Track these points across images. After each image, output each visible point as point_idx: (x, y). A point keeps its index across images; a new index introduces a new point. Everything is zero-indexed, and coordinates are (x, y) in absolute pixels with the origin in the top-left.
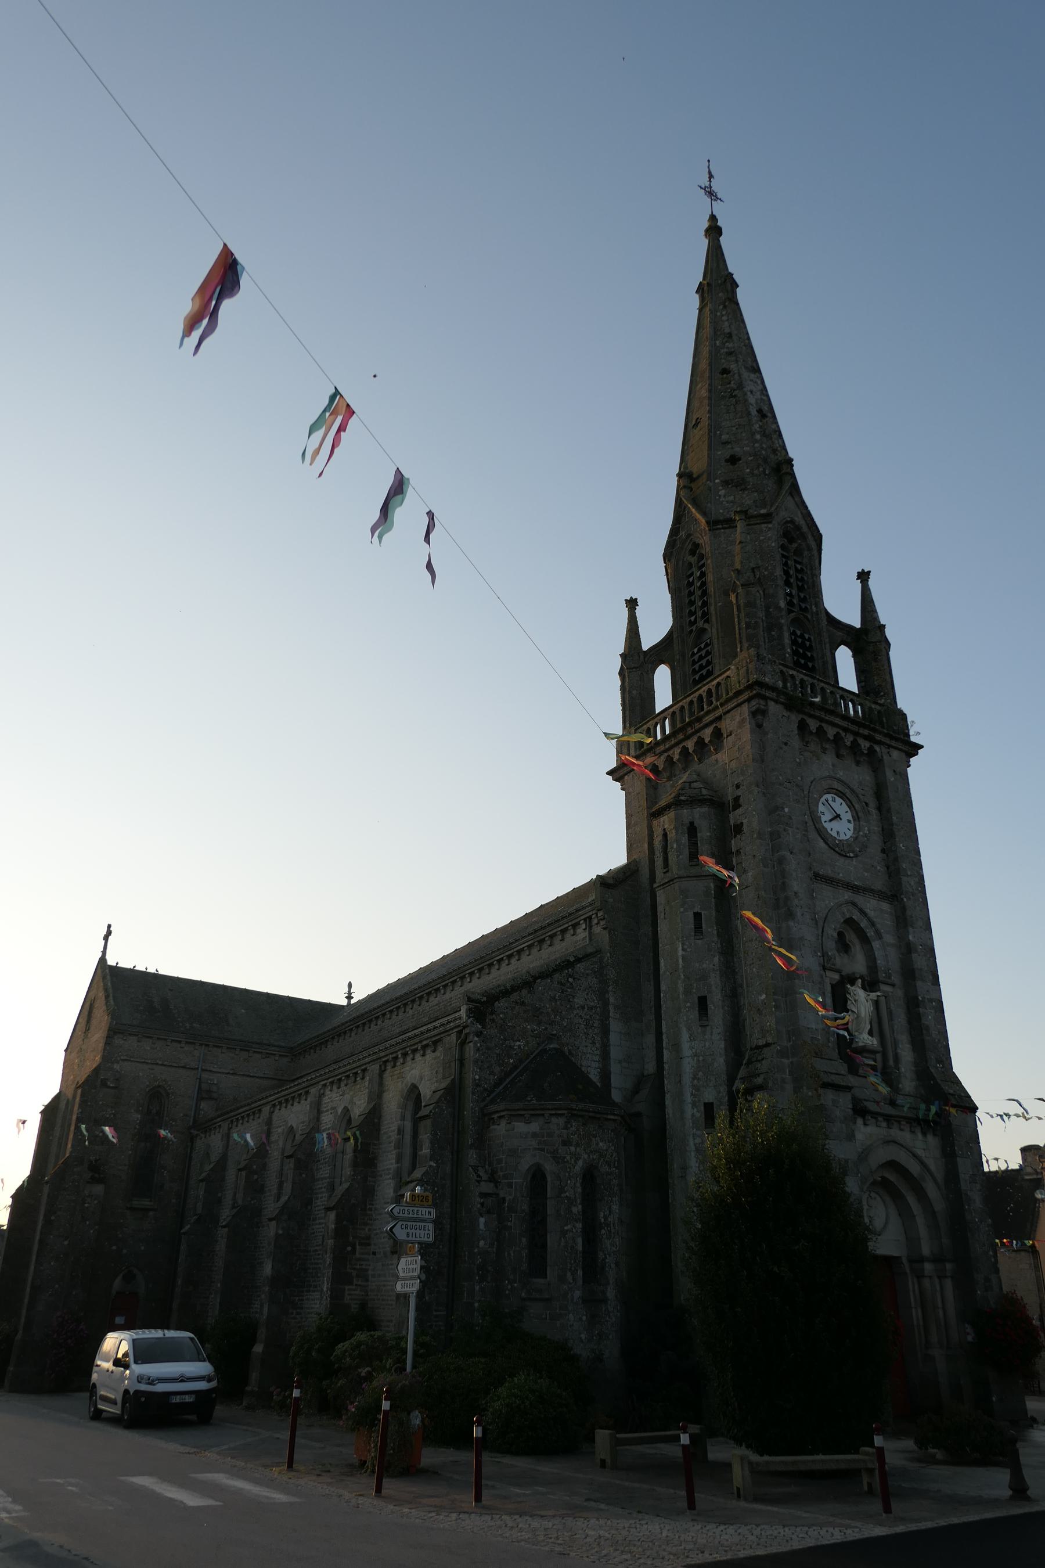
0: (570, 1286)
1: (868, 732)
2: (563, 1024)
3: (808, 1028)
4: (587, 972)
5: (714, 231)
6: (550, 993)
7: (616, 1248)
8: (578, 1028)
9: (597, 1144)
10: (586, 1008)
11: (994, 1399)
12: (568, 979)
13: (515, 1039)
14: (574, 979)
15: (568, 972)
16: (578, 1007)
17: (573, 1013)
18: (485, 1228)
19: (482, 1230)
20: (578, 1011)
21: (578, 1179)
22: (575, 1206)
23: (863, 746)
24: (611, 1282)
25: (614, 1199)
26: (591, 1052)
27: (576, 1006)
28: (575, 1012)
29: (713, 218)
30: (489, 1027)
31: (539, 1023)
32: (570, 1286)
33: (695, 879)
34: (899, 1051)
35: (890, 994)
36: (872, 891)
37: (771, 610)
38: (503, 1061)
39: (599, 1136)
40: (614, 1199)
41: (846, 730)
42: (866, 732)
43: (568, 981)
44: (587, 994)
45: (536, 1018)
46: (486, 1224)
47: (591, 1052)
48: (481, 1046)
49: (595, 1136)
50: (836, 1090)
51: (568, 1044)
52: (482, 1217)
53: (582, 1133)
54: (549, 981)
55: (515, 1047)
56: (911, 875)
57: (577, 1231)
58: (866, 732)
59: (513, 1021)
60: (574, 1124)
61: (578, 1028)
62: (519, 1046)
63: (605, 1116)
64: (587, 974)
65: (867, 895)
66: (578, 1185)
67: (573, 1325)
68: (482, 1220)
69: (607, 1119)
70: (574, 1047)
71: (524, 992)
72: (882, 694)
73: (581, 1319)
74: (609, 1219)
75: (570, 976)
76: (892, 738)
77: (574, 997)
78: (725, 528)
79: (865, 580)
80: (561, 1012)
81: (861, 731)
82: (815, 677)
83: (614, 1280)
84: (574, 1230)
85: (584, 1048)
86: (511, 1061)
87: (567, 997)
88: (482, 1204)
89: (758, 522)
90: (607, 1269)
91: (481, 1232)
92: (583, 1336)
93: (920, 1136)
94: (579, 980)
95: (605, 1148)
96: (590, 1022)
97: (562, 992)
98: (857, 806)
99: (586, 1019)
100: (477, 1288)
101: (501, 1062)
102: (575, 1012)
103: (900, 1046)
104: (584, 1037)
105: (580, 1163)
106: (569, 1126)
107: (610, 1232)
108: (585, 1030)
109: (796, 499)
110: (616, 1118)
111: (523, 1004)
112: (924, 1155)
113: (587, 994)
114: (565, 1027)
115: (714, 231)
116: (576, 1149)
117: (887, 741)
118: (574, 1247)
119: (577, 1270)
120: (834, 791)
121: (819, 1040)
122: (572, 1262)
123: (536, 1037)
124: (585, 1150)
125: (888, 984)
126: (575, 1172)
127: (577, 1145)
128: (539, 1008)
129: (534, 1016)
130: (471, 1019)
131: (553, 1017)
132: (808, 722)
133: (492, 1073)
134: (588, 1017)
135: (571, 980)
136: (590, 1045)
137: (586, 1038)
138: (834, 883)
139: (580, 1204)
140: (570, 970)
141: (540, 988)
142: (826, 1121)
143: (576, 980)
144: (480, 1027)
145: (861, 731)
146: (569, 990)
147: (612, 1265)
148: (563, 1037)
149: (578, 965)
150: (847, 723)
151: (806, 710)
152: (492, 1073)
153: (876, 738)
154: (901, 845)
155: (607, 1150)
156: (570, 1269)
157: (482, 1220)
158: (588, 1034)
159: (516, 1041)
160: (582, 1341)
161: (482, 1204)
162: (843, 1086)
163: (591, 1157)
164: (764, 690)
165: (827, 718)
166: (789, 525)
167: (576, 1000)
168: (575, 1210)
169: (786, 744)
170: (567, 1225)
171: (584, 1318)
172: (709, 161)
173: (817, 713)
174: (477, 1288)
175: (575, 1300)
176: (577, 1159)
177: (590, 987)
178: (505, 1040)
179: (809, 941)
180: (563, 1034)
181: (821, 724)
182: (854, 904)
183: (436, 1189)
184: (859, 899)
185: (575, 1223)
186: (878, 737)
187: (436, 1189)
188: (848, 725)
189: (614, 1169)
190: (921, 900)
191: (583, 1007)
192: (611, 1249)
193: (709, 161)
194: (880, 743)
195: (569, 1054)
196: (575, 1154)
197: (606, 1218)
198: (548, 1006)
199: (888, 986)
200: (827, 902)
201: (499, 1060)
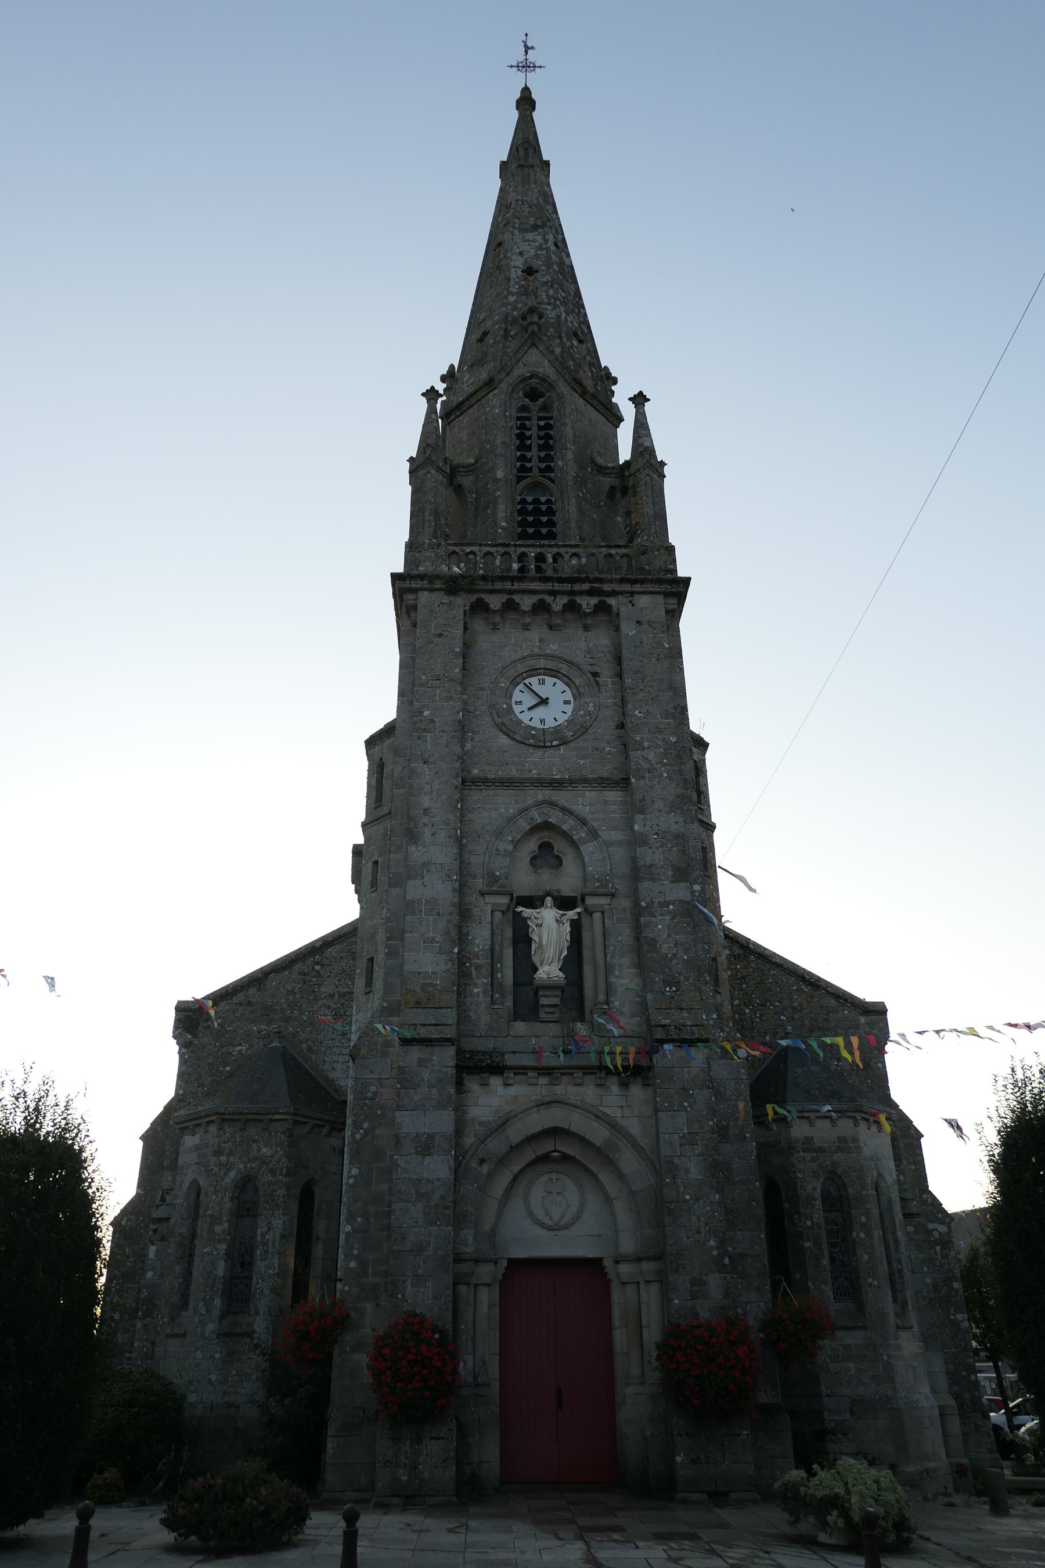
0: (201, 1318)
1: (589, 585)
4: (342, 955)
5: (526, 103)
7: (274, 1270)
9: (259, 1151)
10: (337, 995)
11: (679, 1459)
13: (236, 1044)
14: (322, 966)
16: (325, 997)
17: (318, 1004)
18: (156, 1257)
19: (151, 1260)
20: (324, 1001)
21: (227, 1193)
22: (218, 1224)
23: (584, 606)
24: (261, 1312)
25: (277, 1212)
26: (340, 1044)
28: (320, 1003)
29: (526, 91)
30: (202, 1035)
31: (270, 1022)
32: (201, 1318)
33: (376, 823)
34: (613, 980)
36: (585, 781)
37: (489, 486)
38: (217, 1070)
39: (263, 1141)
40: (277, 1212)
41: (553, 593)
42: (586, 586)
43: (313, 969)
44: (339, 980)
45: (266, 1017)
46: (157, 1252)
47: (340, 1044)
48: (189, 1057)
49: (256, 1141)
51: (307, 1040)
52: (153, 1245)
53: (238, 1140)
55: (234, 1053)
56: (649, 747)
57: (218, 1254)
58: (586, 586)
59: (235, 1025)
60: (228, 1130)
62: (240, 1051)
63: (270, 1117)
64: (341, 958)
65: (580, 788)
66: (227, 1199)
67: (200, 1364)
68: (152, 1249)
69: (271, 1120)
71: (252, 991)
72: (639, 532)
73: (212, 1357)
74: (267, 1237)
75: (317, 963)
76: (633, 582)
77: (320, 986)
78: (458, 417)
79: (641, 404)
80: (301, 1005)
81: (577, 587)
82: (510, 544)
83: (266, 1309)
84: (215, 1253)
85: (330, 1042)
86: (228, 1069)
88: (155, 1231)
89: (485, 393)
90: (257, 1296)
91: (150, 1262)
92: (213, 1377)
93: (615, 1089)
95: (269, 1154)
97: (305, 983)
98: (577, 681)
99: (334, 1009)
100: (139, 1325)
101: (214, 1071)
102: (320, 1003)
103: (616, 973)
105: (233, 1174)
106: (221, 1133)
107: (267, 1252)
109: (541, 348)
110: (286, 1117)
111: (249, 1003)
113: (339, 980)
114: (305, 1021)
115: (526, 103)
116: (228, 1159)
117: (627, 587)
118: (212, 1272)
119: (213, 1300)
120: (542, 671)
122: (208, 1289)
123: (264, 1039)
124: (240, 1158)
126: (224, 1185)
127: (230, 1153)
128: (271, 1006)
129: (263, 1015)
130: (179, 1030)
132: (486, 600)
133: (202, 1085)
134: (338, 1005)
135: (317, 967)
138: (515, 784)
139: (226, 1221)
140: (317, 957)
141: (274, 983)
142: (401, 1088)
144: (190, 1037)
145: (577, 587)
147: (265, 1290)
149: (329, 950)
150: (551, 584)
151: (479, 587)
152: (202, 1085)
153: (605, 589)
154: (637, 712)
155: (272, 1156)
156: (204, 1298)
157: (152, 1249)
159: (237, 1046)
160: (211, 1384)
161: (155, 1231)
162: (436, 1039)
163: (249, 1165)
164: (408, 582)
165: (516, 587)
166: (532, 381)
167: (322, 989)
168: (218, 1229)
169: (440, 635)
170: (206, 1248)
171: (217, 1355)
172: (526, 35)
173: (498, 586)
174: (139, 1325)
175: (207, 1335)
176: (229, 1170)
177: (345, 971)
178: (222, 1046)
181: (510, 597)
182: (552, 804)
183: (141, 1218)
184: (562, 797)
185: (216, 1244)
186: (607, 587)
187: (141, 1218)
188: (553, 586)
190: (665, 775)
191: (332, 996)
192: (266, 1272)
193: (526, 35)
194: (613, 594)
195: (308, 1051)
196: (226, 1165)
197: (263, 1235)
198: (283, 1001)
201: (212, 1070)
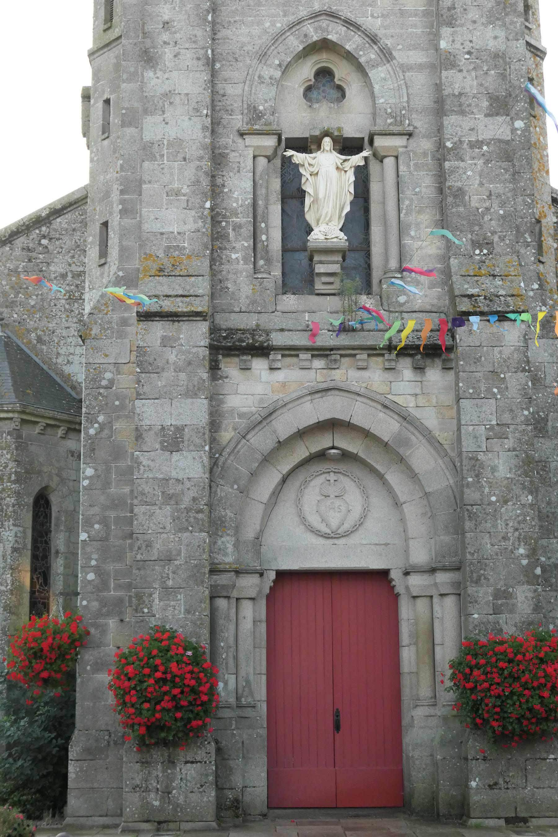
2: (29, 304)
3: (162, 234)
4: (74, 226)
6: (8, 265)
8: (55, 305)
10: (70, 275)
11: (473, 784)
12: (40, 241)
14: (50, 239)
15: (40, 231)
16: (55, 278)
25: (6, 523)
27: (53, 276)
35: (401, 150)
40: (6, 523)
43: (40, 244)
50: (174, 321)
51: (36, 329)
54: (8, 249)
61: (55, 305)
64: (74, 230)
70: (47, 331)
75: (44, 237)
80: (27, 288)
87: (38, 265)
94: (58, 239)
96: (76, 294)
97: (30, 260)
103: (413, 233)
104: (64, 316)
108: (67, 306)
112: (412, 404)
121: (184, 248)
125: (394, 134)
131: (12, 296)
134: (72, 287)
135: (44, 242)
136: (73, 325)
137: (68, 316)
140: (44, 229)
143: (53, 240)
146: (41, 256)
148: (28, 321)
149: (58, 220)
158: (73, 311)
179: (187, 94)
180: (29, 317)
189: (9, 484)
195: (38, 342)
199: (396, 137)
200: (267, 25)
